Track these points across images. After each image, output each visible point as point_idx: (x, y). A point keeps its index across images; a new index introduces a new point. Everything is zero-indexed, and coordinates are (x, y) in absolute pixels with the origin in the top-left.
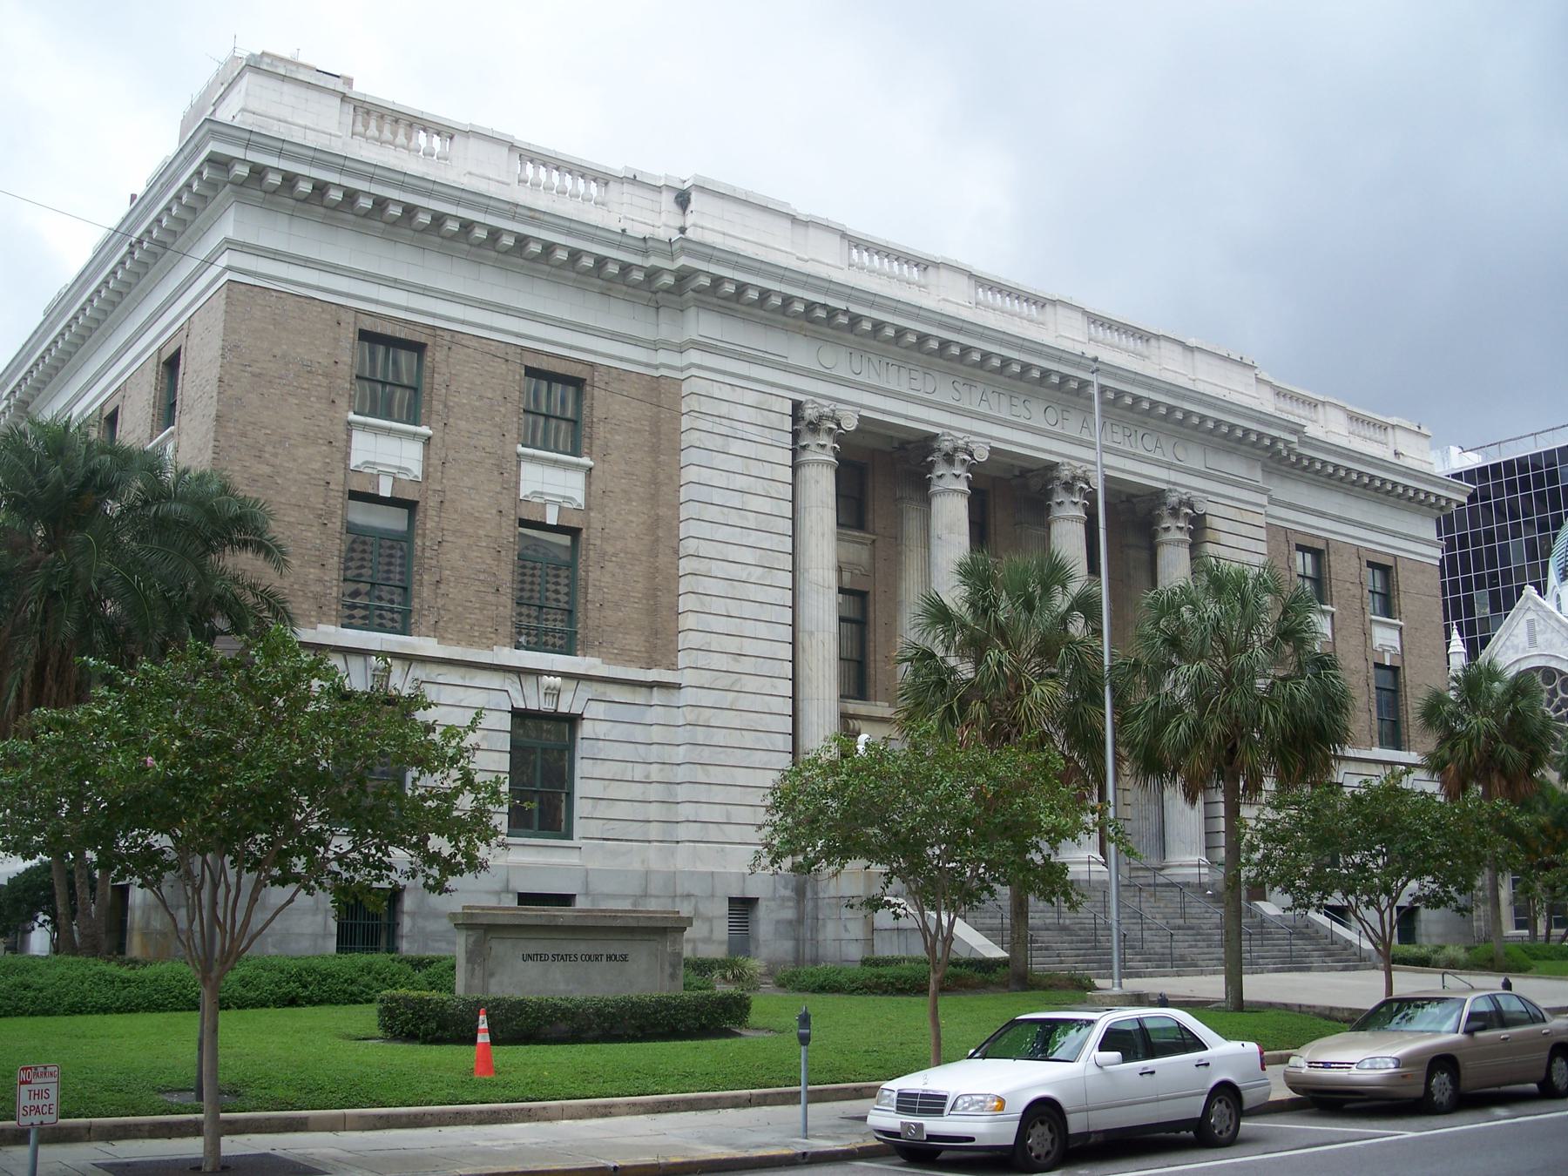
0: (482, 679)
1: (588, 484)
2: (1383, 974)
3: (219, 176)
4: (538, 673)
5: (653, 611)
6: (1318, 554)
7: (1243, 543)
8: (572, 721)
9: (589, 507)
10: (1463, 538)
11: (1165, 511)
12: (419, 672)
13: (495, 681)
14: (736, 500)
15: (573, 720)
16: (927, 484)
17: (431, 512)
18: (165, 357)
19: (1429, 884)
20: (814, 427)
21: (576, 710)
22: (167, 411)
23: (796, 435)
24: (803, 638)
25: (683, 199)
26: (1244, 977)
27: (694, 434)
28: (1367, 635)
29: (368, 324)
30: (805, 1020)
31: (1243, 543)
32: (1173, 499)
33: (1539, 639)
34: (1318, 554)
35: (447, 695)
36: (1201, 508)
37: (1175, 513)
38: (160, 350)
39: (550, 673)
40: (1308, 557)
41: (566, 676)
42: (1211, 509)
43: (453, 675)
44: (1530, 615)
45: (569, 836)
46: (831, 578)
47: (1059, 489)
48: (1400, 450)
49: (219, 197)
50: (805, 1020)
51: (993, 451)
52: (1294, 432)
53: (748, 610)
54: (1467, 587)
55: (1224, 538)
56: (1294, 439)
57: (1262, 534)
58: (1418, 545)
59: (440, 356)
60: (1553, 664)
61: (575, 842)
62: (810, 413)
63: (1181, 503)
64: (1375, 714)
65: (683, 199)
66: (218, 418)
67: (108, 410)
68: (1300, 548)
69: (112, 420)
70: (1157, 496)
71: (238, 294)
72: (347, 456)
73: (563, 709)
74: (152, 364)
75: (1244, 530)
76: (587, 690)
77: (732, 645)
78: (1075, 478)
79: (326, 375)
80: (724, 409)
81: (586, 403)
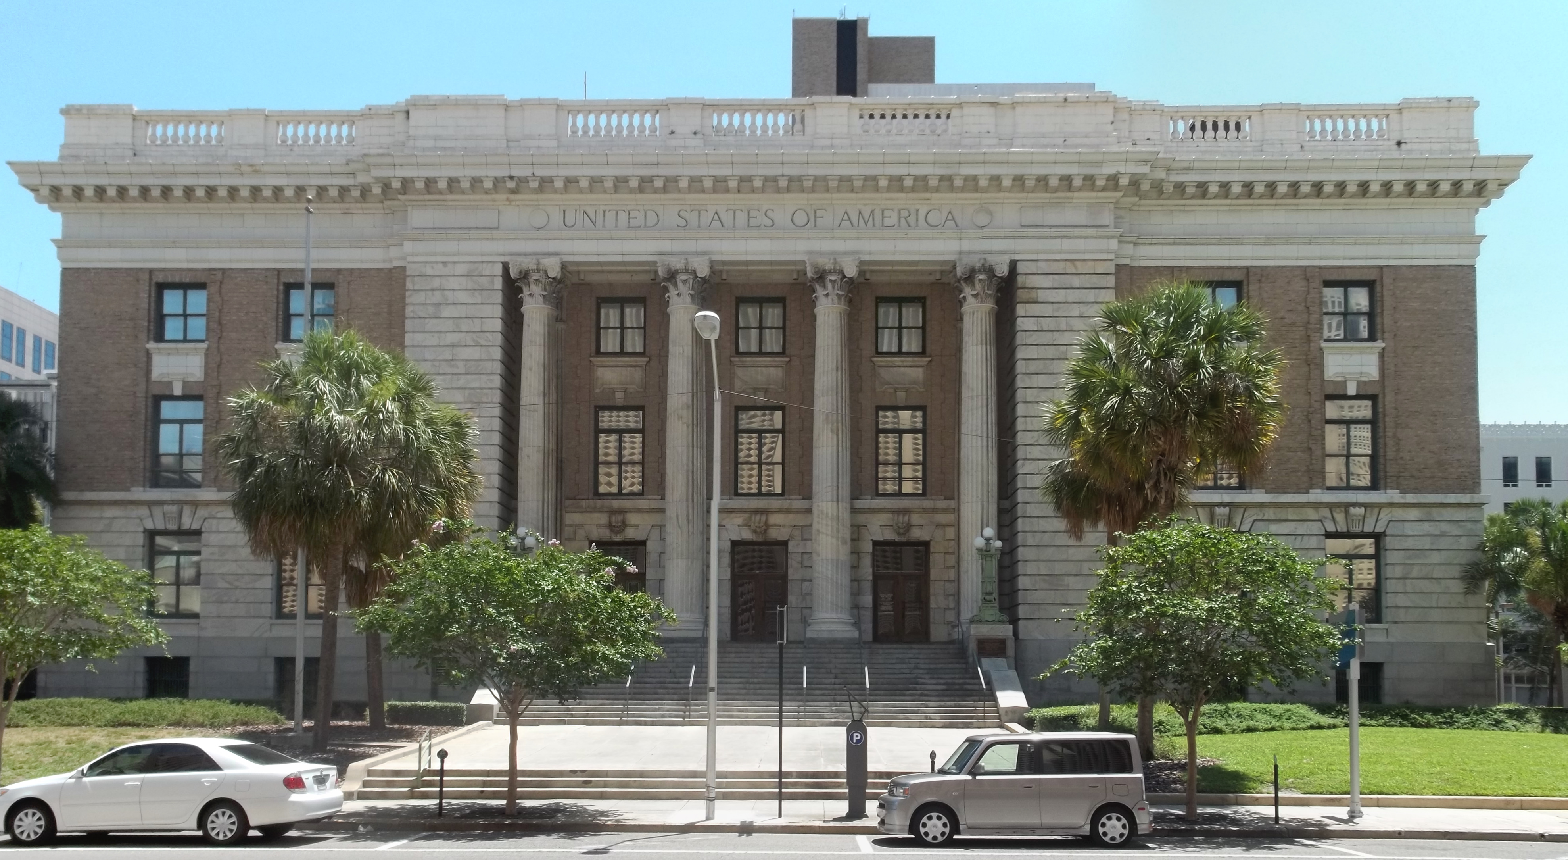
12: (202, 512)
13: (1311, 514)
21: (195, 527)
27: (416, 302)
29: (160, 278)
34: (161, 287)
39: (1355, 505)
47: (964, 285)
48: (1406, 136)
51: (712, 264)
55: (1042, 295)
75: (1076, 281)
79: (131, 319)
80: (436, 283)
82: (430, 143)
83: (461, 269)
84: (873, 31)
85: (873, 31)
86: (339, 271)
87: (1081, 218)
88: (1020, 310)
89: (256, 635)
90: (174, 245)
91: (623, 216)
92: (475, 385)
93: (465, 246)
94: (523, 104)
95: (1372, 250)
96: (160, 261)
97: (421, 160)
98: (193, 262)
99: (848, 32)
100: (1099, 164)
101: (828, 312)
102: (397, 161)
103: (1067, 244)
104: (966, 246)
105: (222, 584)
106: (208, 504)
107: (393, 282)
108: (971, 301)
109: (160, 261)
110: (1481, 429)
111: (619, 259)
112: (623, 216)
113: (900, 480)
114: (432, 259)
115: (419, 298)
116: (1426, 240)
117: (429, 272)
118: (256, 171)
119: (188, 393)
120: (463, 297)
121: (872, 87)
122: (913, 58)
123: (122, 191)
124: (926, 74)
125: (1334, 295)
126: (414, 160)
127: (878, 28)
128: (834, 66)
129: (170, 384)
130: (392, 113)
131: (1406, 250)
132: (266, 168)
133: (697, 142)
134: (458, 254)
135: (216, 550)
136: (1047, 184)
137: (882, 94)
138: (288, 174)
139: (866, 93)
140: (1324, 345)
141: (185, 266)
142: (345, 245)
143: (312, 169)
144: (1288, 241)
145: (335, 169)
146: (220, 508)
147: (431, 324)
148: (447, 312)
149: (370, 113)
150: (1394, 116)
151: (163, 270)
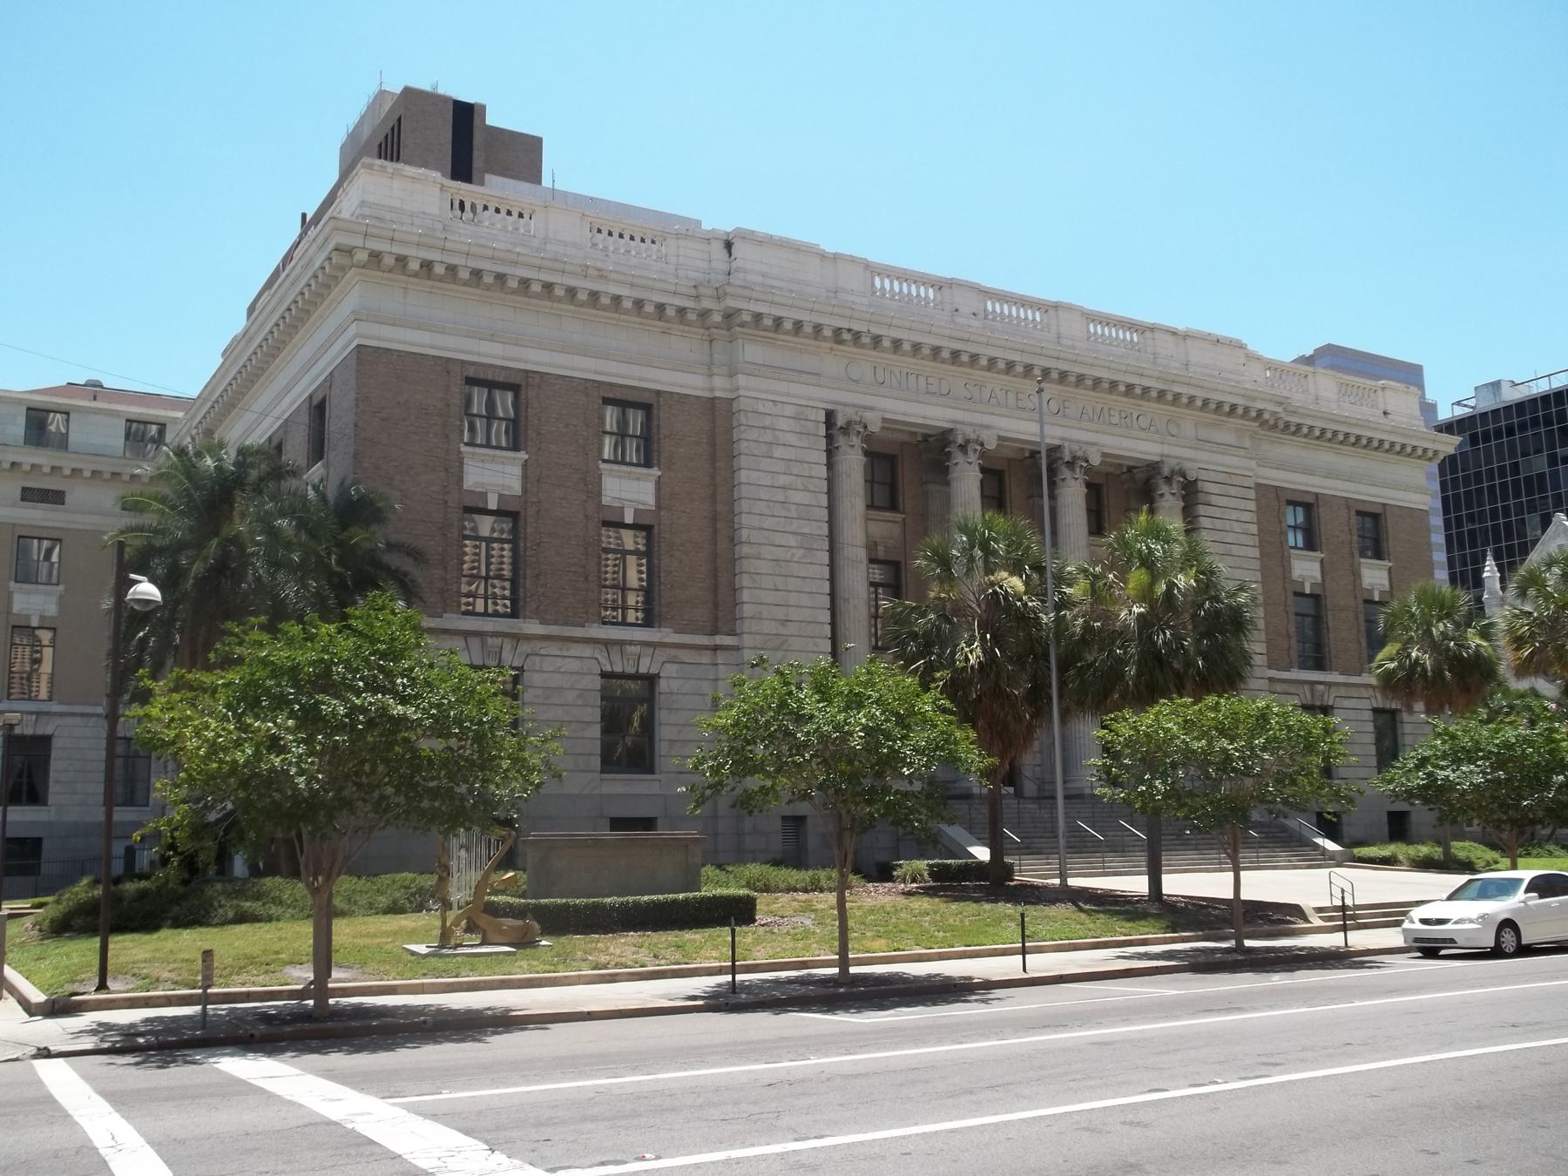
0: (576, 650)
1: (525, 477)
2: (1231, 874)
3: (345, 261)
4: (622, 643)
5: (715, 589)
6: (1308, 508)
7: (1233, 503)
8: (651, 680)
9: (659, 507)
10: (1478, 475)
11: (1161, 482)
12: (524, 647)
13: (587, 651)
14: (780, 496)
15: (651, 680)
16: (946, 470)
17: (530, 520)
18: (315, 402)
20: (845, 430)
22: (318, 449)
23: (829, 437)
24: (841, 604)
25: (729, 245)
26: (1164, 877)
27: (748, 440)
28: (1356, 574)
29: (471, 373)
30: (1023, 915)
31: (1233, 503)
32: (1166, 471)
34: (1308, 508)
35: (548, 665)
36: (1191, 476)
38: (311, 397)
40: (1300, 510)
42: (1203, 475)
43: (552, 649)
45: (652, 772)
46: (862, 554)
48: (1389, 409)
49: (348, 276)
50: (1023, 915)
52: (1281, 404)
54: (1520, 511)
56: (1280, 409)
57: (1252, 494)
58: (1414, 490)
59: (532, 393)
62: (840, 422)
63: (1173, 472)
64: (1364, 644)
65: (729, 245)
66: (355, 455)
67: (275, 442)
68: (1289, 503)
69: (279, 447)
70: (1153, 468)
71: (365, 356)
72: (460, 479)
73: (643, 670)
74: (306, 405)
75: (1233, 491)
76: (662, 655)
77: (780, 613)
78: (968, 441)
80: (768, 421)
81: (655, 423)
82: (759, 279)
83: (789, 410)
84: (491, 120)
85: (491, 120)
86: (658, 393)
87: (1230, 438)
88: (1202, 510)
89: (586, 792)
90: (492, 338)
91: (922, 380)
92: (806, 530)
93: (795, 388)
94: (836, 257)
96: (519, 360)
97: (776, 299)
98: (509, 359)
99: (465, 115)
100: (1254, 399)
102: (755, 295)
103: (1227, 460)
104: (1167, 450)
107: (718, 415)
108: (1168, 496)
109: (519, 360)
111: (921, 421)
112: (922, 380)
113: (625, 608)
114: (763, 396)
115: (753, 434)
116: (1395, 487)
117: (761, 409)
118: (602, 275)
119: (640, 522)
120: (792, 439)
121: (488, 177)
122: (522, 156)
123: (1206, 402)
124: (534, 175)
125: (479, 397)
126: (769, 297)
127: (493, 119)
128: (449, 147)
129: (484, 495)
130: (708, 238)
131: (1401, 495)
132: (613, 276)
133: (975, 323)
134: (788, 395)
135: (539, 692)
136: (405, 265)
137: (495, 187)
138: (632, 285)
139: (482, 183)
140: (463, 448)
142: (669, 368)
143: (658, 285)
145: (679, 289)
146: (545, 644)
147: (765, 463)
148: (779, 452)
151: (473, 363)
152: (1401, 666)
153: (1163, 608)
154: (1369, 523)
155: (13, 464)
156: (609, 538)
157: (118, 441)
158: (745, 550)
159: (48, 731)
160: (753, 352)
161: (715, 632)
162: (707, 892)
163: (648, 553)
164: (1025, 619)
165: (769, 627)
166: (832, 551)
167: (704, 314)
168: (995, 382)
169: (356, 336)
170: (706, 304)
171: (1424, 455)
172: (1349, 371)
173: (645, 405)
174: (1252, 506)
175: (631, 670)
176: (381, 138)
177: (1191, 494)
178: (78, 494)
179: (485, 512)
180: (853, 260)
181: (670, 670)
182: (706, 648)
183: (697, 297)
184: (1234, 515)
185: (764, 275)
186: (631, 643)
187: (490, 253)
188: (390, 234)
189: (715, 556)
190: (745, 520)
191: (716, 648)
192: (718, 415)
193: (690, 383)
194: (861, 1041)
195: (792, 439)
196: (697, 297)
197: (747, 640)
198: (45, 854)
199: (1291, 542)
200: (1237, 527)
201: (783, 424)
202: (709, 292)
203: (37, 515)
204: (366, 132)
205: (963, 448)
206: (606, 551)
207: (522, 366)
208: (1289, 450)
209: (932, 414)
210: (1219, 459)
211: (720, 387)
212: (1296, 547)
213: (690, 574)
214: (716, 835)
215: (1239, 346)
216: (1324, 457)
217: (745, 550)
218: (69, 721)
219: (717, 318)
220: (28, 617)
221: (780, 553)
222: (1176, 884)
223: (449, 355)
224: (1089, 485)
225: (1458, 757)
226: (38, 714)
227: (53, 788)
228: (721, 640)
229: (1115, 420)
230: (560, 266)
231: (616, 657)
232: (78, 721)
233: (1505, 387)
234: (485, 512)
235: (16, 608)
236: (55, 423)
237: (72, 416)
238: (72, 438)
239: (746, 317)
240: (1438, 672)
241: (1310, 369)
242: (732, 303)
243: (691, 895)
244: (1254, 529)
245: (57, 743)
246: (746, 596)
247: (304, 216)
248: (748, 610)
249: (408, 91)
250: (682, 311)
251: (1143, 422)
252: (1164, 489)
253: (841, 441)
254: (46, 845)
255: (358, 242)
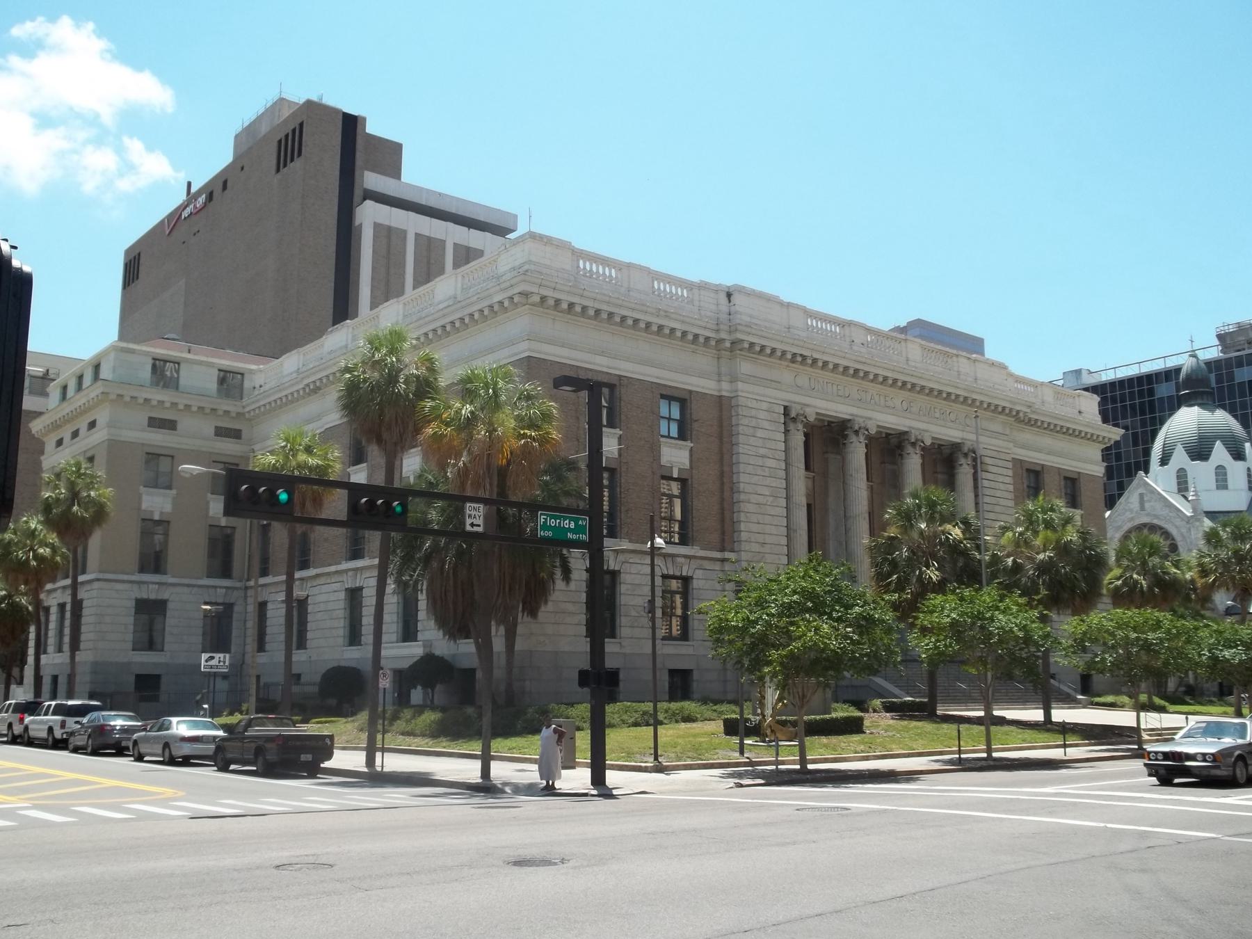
1: (691, 455)
2: (651, 728)
3: (523, 300)
5: (723, 521)
12: (621, 557)
19: (1221, 419)
20: (794, 420)
21: (690, 574)
25: (729, 295)
27: (744, 425)
32: (966, 450)
33: (1147, 505)
37: (966, 455)
41: (685, 556)
44: (1141, 490)
48: (1083, 409)
53: (768, 519)
55: (991, 469)
57: (1010, 465)
60: (1155, 521)
61: (253, 745)
62: (793, 415)
65: (729, 295)
67: (79, 374)
68: (663, 397)
70: (956, 447)
73: (684, 574)
75: (1000, 463)
76: (694, 564)
77: (760, 538)
78: (917, 440)
80: (753, 413)
82: (748, 319)
90: (602, 354)
94: (789, 305)
95: (1074, 463)
100: (1014, 403)
101: (857, 453)
105: (634, 613)
106: (623, 551)
107: (723, 407)
108: (965, 466)
110: (23, 414)
120: (766, 425)
130: (716, 289)
133: (863, 350)
138: (683, 322)
141: (605, 370)
142: (695, 375)
144: (1040, 451)
147: (752, 441)
148: (760, 433)
149: (703, 286)
150: (696, 291)
152: (1125, 583)
153: (1063, 550)
154: (1032, 476)
155: (146, 400)
156: (664, 487)
157: (213, 385)
158: (742, 497)
159: (165, 596)
160: (745, 367)
161: (722, 550)
162: (834, 715)
163: (684, 496)
164: (964, 553)
165: (755, 547)
166: (788, 498)
167: (720, 341)
168: (874, 389)
169: (529, 350)
170: (723, 335)
171: (1091, 438)
172: (931, 340)
173: (683, 400)
174: (1010, 473)
175: (678, 574)
176: (281, 135)
177: (977, 464)
178: (185, 423)
179: (671, 478)
180: (798, 307)
181: (626, 567)
182: (718, 560)
183: (718, 331)
184: (1001, 479)
185: (751, 316)
186: (678, 556)
187: (607, 299)
188: (553, 285)
189: (722, 500)
190: (743, 478)
191: (723, 560)
192: (723, 407)
193: (704, 385)
194: (1044, 783)
195: (766, 425)
196: (718, 331)
197: (744, 556)
198: (163, 687)
199: (664, 431)
200: (1002, 486)
201: (762, 415)
202: (726, 328)
203: (158, 438)
204: (264, 129)
205: (857, 432)
206: (664, 494)
207: (617, 373)
208: (1027, 436)
209: (839, 409)
210: (1001, 447)
211: (725, 389)
212: (669, 437)
213: (706, 513)
214: (725, 681)
215: (1003, 367)
216: (1047, 441)
217: (742, 497)
218: (178, 589)
219: (728, 344)
220: (152, 512)
221: (761, 499)
222: (1059, 715)
223: (542, 356)
224: (806, 435)
225: (1229, 644)
226: (160, 584)
227: (168, 638)
228: (727, 555)
229: (937, 415)
230: (644, 308)
231: (670, 565)
232: (186, 590)
233: (1084, 374)
234: (671, 478)
235: (144, 506)
236: (169, 370)
237: (182, 365)
238: (182, 382)
239: (746, 345)
240: (1150, 588)
241: (903, 336)
242: (739, 336)
243: (827, 716)
244: (1011, 488)
245: (170, 606)
246: (743, 526)
247: (189, 184)
248: (744, 536)
249: (309, 103)
250: (707, 339)
251: (953, 417)
252: (962, 461)
253: (791, 426)
254: (164, 680)
255: (535, 289)
